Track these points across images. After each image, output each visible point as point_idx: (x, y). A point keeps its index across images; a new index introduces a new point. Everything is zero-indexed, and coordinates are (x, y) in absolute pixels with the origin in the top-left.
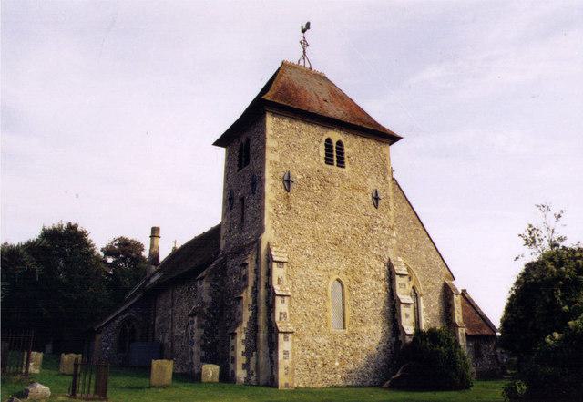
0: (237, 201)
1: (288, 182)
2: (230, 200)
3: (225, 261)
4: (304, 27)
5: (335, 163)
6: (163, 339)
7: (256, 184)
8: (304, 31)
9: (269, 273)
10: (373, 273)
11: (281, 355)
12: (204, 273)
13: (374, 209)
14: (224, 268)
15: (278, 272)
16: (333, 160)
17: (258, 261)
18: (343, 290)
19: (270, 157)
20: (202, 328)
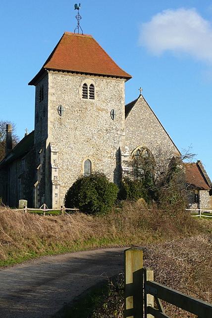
0: (39, 119)
1: (60, 111)
5: (89, 97)
6: (13, 192)
12: (25, 157)
13: (112, 121)
15: (53, 157)
16: (87, 96)
18: (91, 164)
20: (24, 184)
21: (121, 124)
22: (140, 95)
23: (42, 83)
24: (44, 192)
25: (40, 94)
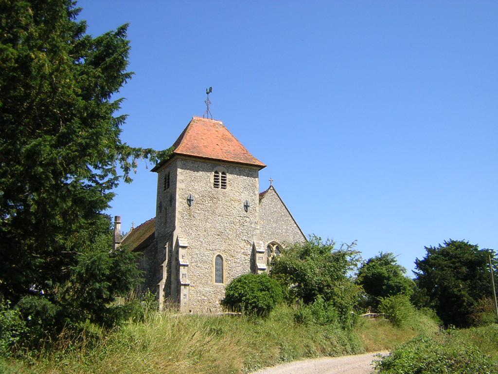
0: (163, 209)
1: (189, 201)
2: (160, 207)
3: (157, 244)
4: (208, 91)
7: (172, 200)
8: (208, 93)
9: (177, 253)
10: (243, 251)
11: (182, 296)
13: (245, 213)
14: (156, 248)
15: (182, 270)
17: (171, 245)
19: (179, 185)
21: (255, 217)
22: (270, 187)
23: (167, 170)
24: (170, 292)
25: (165, 181)
